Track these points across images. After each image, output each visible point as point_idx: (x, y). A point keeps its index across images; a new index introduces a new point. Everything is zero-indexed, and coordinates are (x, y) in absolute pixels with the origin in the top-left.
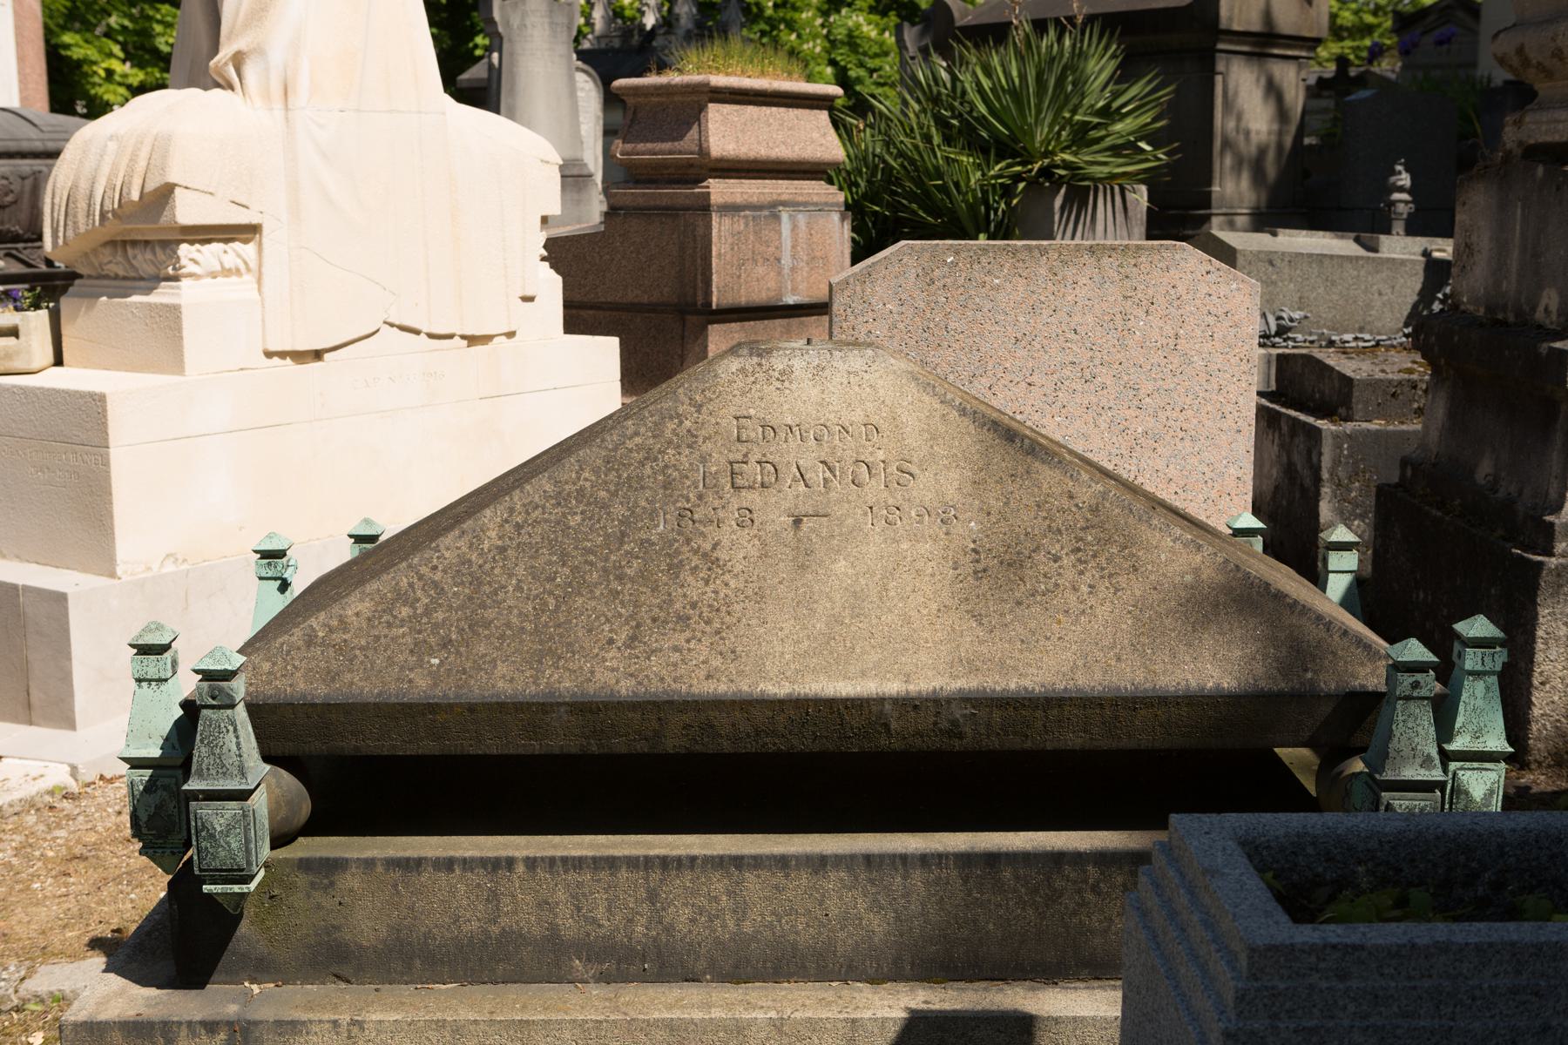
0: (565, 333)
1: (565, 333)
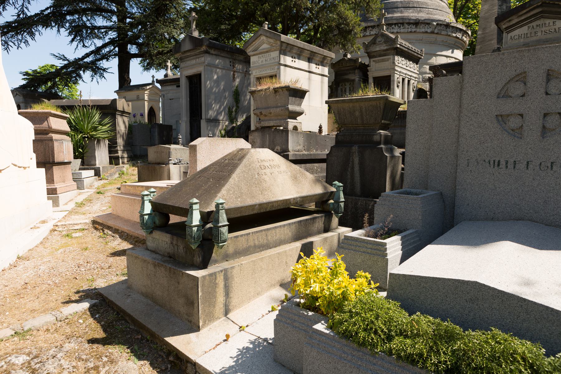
0: (37, 167)
1: (37, 167)
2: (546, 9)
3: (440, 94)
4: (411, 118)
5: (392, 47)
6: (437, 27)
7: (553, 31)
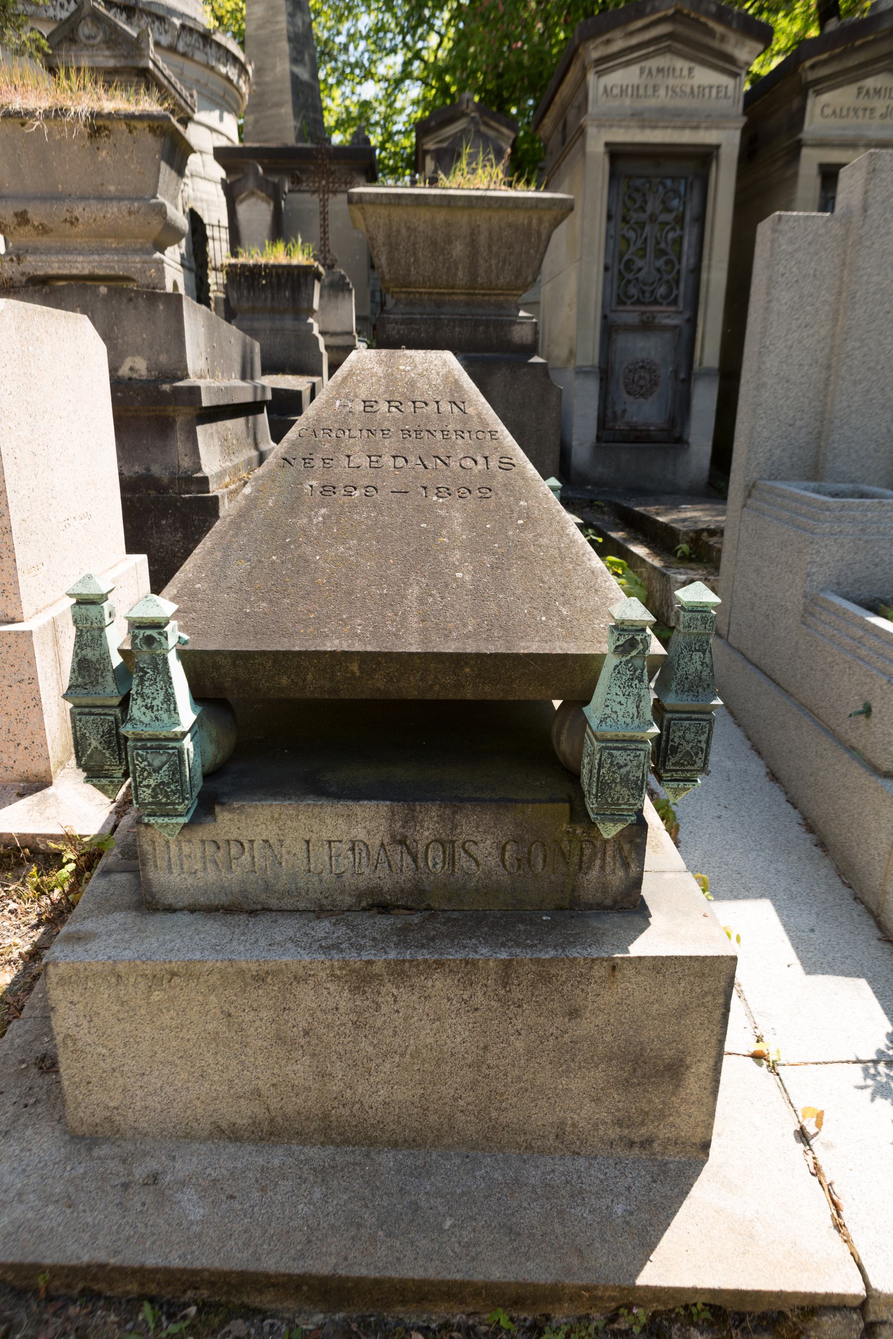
2: (680, 29)
3: (884, 202)
4: (782, 270)
5: (130, 63)
6: (183, 35)
7: (688, 90)
